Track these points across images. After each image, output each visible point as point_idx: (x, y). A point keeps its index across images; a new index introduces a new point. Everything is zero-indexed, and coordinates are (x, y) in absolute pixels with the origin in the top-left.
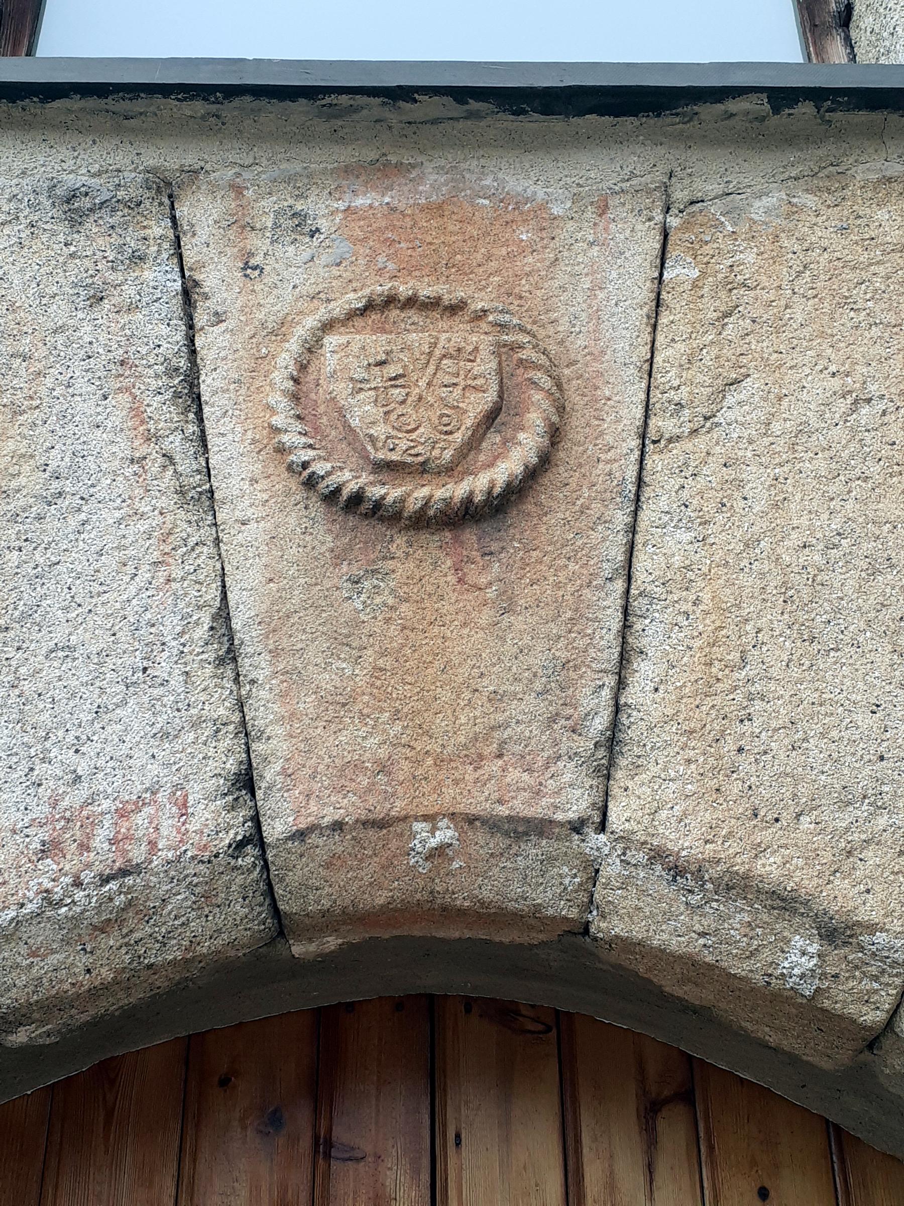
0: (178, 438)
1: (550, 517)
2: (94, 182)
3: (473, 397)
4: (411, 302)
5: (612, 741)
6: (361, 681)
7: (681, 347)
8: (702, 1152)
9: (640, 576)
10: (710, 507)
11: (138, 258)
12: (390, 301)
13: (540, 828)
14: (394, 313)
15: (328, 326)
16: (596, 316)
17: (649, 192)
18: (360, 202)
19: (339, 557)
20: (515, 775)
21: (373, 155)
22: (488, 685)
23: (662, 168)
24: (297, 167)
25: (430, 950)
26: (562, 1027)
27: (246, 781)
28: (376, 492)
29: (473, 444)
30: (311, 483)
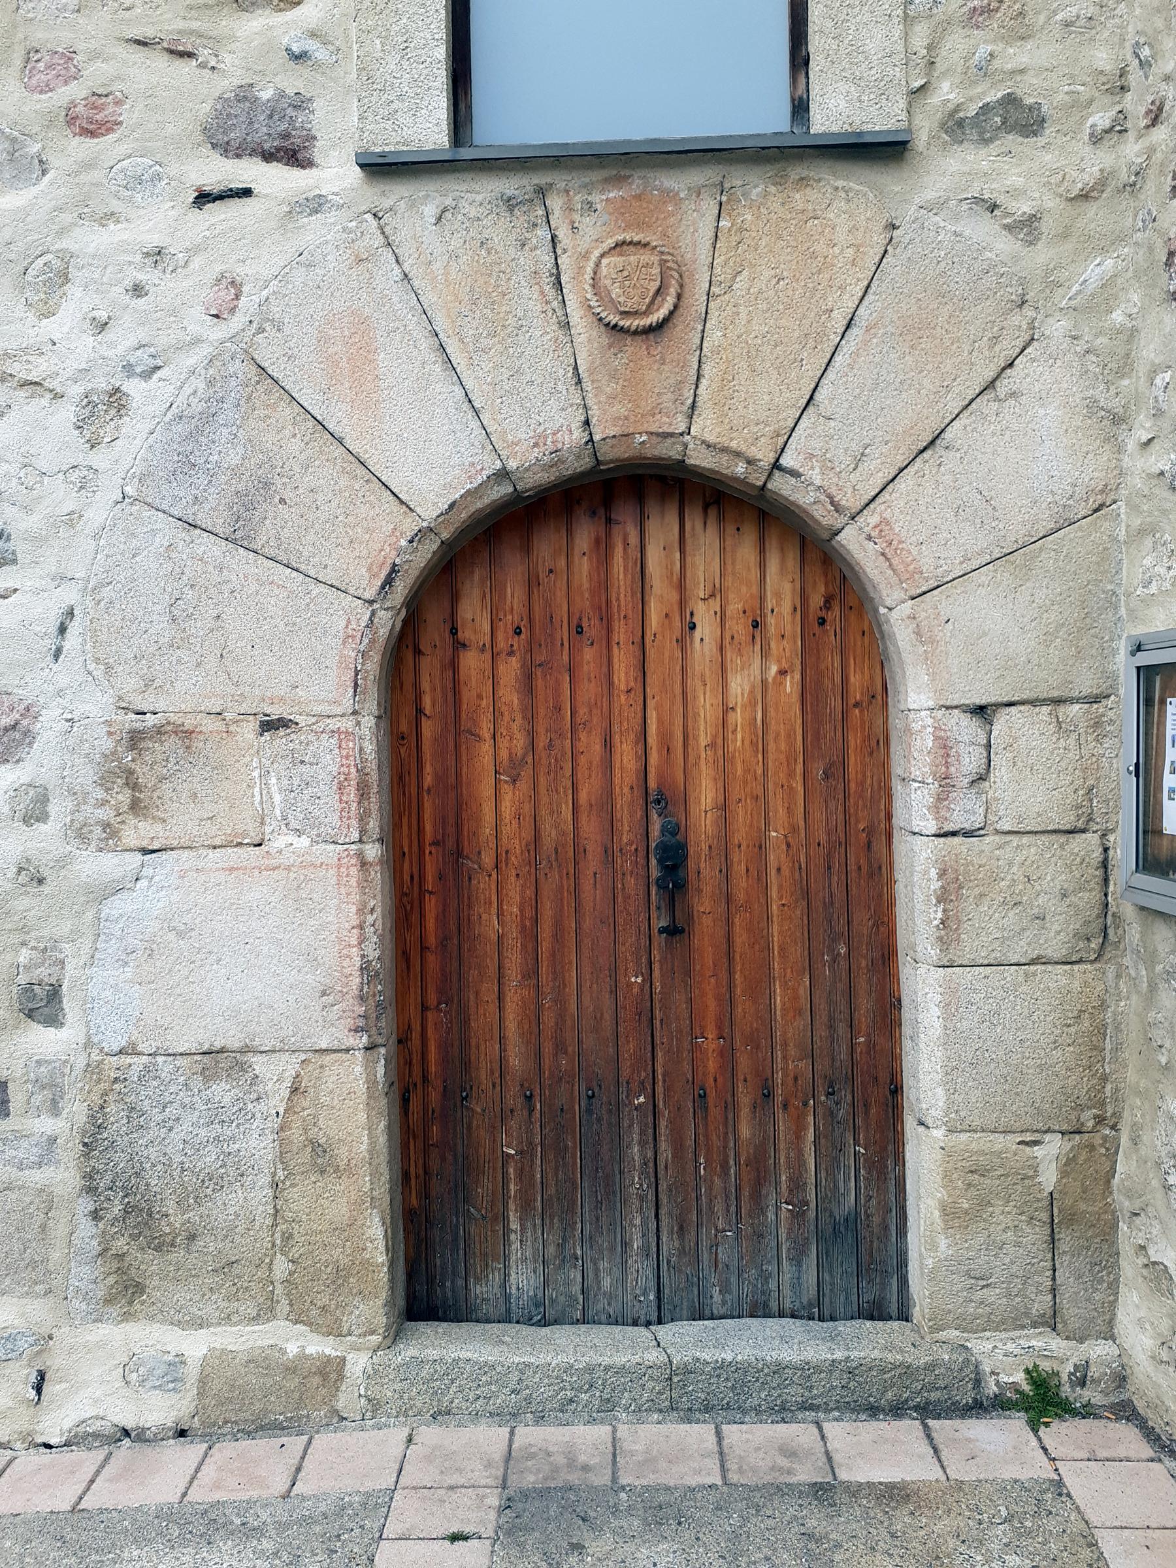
0: (556, 302)
1: (678, 328)
2: (516, 192)
3: (652, 283)
4: (631, 243)
5: (693, 407)
6: (619, 389)
7: (722, 258)
8: (721, 519)
9: (705, 349)
10: (728, 323)
11: (535, 225)
12: (624, 243)
13: (671, 435)
14: (625, 247)
15: (602, 256)
16: (694, 245)
17: (716, 186)
18: (611, 195)
19: (610, 346)
20: (665, 419)
21: (615, 172)
22: (657, 390)
23: (721, 175)
24: (587, 180)
25: (639, 466)
26: (681, 482)
27: (587, 423)
28: (621, 323)
29: (652, 302)
30: (600, 320)
